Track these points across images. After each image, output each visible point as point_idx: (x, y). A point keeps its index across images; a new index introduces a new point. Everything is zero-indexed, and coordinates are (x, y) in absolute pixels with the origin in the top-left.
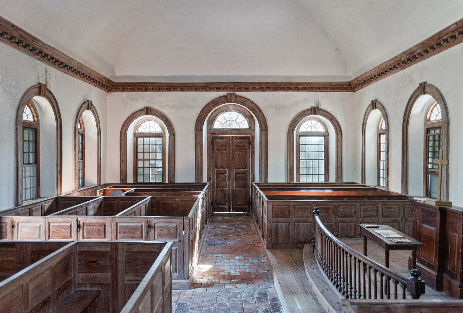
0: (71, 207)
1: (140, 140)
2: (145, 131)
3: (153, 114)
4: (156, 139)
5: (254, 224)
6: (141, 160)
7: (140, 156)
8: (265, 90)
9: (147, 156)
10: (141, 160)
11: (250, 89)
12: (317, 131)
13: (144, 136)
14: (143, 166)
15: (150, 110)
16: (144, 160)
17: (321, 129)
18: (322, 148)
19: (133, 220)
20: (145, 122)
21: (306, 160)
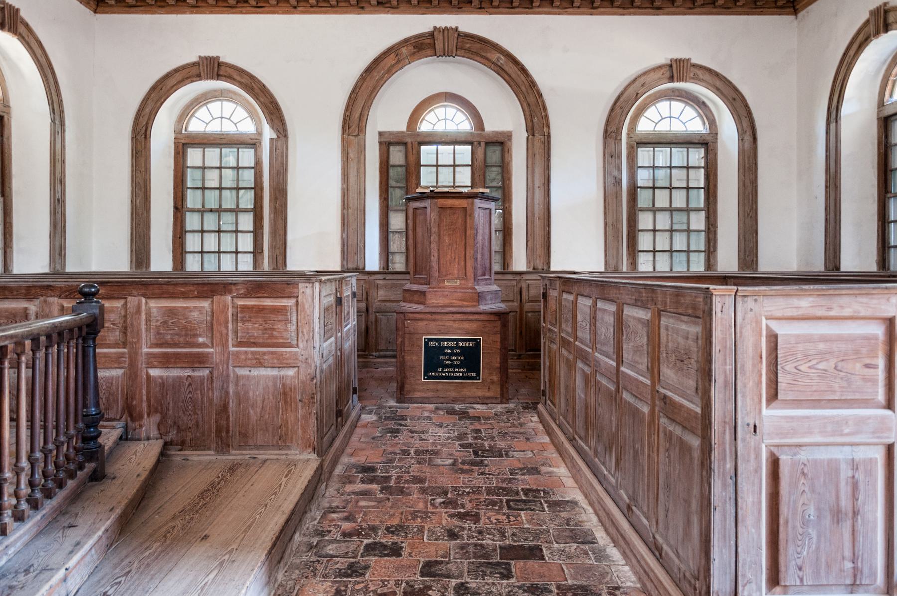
0: (767, 389)
1: (194, 157)
2: (207, 129)
3: (225, 76)
4: (699, 168)
5: (116, 345)
6: (245, 211)
7: (193, 200)
8: (498, 7)
9: (212, 200)
10: (245, 211)
11: (574, 5)
12: (685, 129)
13: (205, 141)
14: (652, 253)
15: (216, 65)
16: (203, 211)
17: (696, 125)
18: (698, 178)
19: (250, 371)
20: (459, 112)
21: (220, 189)
